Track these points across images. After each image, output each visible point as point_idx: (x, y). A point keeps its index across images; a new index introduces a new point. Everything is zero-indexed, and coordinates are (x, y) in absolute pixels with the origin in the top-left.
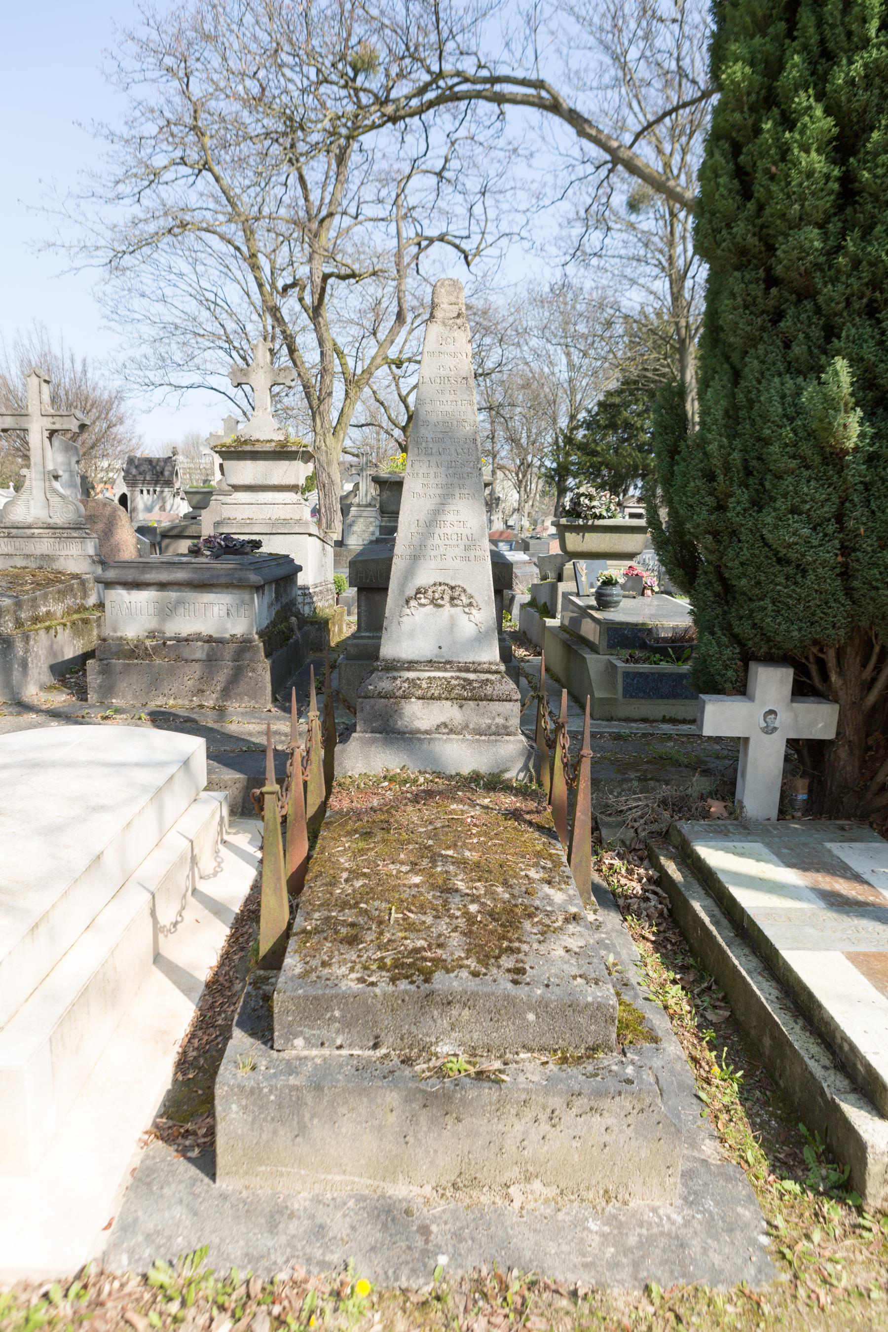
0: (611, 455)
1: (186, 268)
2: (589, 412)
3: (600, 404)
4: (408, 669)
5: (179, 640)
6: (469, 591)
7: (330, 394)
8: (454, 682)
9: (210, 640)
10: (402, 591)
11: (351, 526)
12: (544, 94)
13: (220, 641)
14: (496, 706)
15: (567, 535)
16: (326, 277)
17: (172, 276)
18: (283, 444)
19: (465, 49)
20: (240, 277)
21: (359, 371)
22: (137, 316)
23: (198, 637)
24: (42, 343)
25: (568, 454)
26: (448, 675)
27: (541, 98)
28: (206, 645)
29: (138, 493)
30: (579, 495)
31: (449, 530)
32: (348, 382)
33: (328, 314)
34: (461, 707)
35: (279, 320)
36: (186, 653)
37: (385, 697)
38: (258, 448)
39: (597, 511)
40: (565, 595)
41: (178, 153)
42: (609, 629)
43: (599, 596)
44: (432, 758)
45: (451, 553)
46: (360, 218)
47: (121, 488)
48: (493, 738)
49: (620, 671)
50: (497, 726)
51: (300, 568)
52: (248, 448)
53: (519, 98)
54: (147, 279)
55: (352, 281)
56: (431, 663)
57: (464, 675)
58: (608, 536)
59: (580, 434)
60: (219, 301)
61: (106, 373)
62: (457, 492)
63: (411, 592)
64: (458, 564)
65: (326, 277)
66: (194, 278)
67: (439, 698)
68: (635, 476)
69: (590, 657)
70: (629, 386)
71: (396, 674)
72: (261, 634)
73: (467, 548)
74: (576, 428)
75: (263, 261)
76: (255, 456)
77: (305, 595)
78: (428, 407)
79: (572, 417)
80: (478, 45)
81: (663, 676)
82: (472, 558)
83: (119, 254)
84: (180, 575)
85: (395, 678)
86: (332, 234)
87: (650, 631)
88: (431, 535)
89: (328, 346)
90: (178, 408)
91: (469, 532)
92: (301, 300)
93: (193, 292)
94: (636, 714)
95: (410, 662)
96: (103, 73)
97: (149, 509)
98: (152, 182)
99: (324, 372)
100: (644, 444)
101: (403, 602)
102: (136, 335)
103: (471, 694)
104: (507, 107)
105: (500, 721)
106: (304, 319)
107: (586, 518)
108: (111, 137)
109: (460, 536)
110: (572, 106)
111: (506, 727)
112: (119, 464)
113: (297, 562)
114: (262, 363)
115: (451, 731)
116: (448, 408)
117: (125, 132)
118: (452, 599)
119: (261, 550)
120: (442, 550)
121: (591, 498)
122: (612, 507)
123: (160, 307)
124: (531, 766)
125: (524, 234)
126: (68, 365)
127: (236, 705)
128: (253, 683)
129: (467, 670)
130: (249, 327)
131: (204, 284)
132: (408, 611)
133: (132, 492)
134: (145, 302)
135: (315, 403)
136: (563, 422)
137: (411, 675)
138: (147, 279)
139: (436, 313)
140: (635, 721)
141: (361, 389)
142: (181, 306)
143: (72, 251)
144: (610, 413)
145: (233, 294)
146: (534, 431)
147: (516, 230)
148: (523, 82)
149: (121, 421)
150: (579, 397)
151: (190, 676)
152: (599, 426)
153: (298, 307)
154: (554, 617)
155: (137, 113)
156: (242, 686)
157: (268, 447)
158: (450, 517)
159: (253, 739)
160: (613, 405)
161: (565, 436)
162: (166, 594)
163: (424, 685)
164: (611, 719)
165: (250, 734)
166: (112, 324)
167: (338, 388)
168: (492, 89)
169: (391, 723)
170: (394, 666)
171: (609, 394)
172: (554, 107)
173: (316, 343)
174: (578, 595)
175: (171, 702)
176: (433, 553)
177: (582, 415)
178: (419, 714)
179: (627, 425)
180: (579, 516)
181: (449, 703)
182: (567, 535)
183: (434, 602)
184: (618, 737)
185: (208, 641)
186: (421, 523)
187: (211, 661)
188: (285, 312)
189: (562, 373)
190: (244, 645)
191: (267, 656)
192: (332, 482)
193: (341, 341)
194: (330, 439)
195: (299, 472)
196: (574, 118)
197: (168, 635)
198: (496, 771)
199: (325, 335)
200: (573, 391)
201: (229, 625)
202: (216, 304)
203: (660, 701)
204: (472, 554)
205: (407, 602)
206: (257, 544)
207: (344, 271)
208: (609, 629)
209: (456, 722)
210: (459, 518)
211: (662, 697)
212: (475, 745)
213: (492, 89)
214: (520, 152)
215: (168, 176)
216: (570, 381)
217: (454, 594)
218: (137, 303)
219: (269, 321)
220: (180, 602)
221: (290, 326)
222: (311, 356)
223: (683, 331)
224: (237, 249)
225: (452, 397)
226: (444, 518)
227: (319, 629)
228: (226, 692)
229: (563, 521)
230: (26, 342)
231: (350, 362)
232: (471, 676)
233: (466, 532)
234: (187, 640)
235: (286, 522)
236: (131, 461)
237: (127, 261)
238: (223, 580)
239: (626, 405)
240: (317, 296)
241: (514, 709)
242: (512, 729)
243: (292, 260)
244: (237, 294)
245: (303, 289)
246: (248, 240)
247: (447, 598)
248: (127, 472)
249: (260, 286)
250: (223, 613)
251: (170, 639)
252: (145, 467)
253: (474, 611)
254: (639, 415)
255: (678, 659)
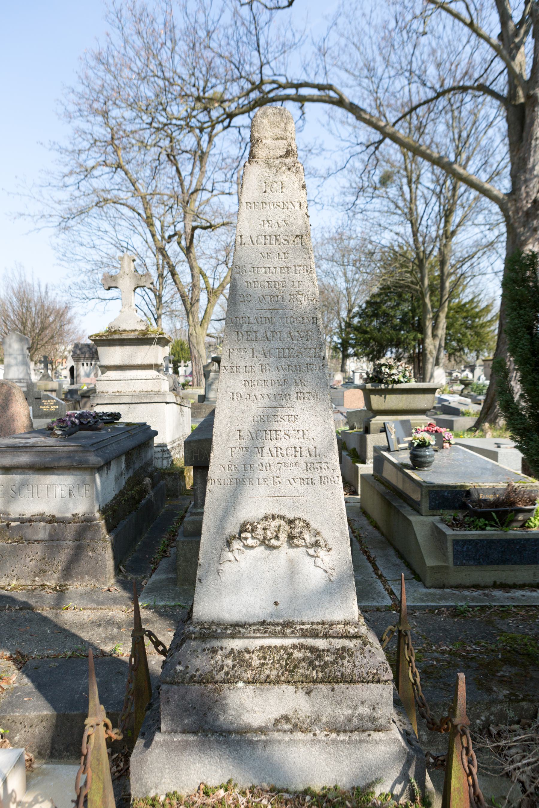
0: (376, 334)
1: (109, 228)
2: (360, 307)
3: (367, 302)
4: (233, 636)
5: (22, 521)
6: (314, 525)
7: (198, 301)
8: (298, 654)
9: (52, 520)
10: (221, 529)
11: (210, 385)
12: (332, 94)
13: (62, 521)
14: (359, 691)
15: (372, 397)
16: (194, 229)
17: (100, 233)
18: (144, 333)
19: (278, 73)
20: (143, 233)
21: (216, 286)
22: (78, 257)
23: (41, 518)
24: (21, 276)
25: (348, 333)
26: (288, 642)
27: (330, 97)
28: (49, 525)
29: (80, 365)
30: (381, 365)
31: (283, 443)
32: (209, 293)
33: (196, 251)
34: (308, 693)
35: (165, 256)
36: (29, 533)
37: (200, 682)
38: (124, 336)
39: (396, 378)
40: (376, 449)
41: (103, 158)
42: (430, 492)
43: (414, 457)
44: (271, 767)
45: (287, 474)
46: (215, 192)
47: (70, 363)
48: (356, 736)
49: (449, 539)
50: (361, 718)
51: (156, 433)
52: (117, 337)
53: (315, 98)
54: (84, 235)
55: (210, 230)
56: (264, 626)
57: (310, 642)
58: (404, 397)
59: (356, 321)
60: (129, 247)
61: (59, 292)
62: (293, 390)
63: (232, 529)
64: (298, 488)
65: (194, 229)
66: (114, 234)
67: (277, 682)
68: (391, 346)
69: (414, 519)
70: (385, 290)
71: (216, 644)
72: (103, 511)
73: (309, 467)
74: (353, 317)
75: (158, 224)
76: (122, 342)
77: (163, 451)
78: (250, 277)
79: (349, 311)
80: (286, 71)
81: (490, 543)
82: (317, 480)
83: (65, 219)
84: (24, 459)
85: (214, 651)
86: (197, 203)
87: (468, 493)
88: (259, 450)
89: (196, 271)
90: (104, 313)
91: (310, 444)
92: (179, 243)
93: (114, 242)
94: (467, 581)
95: (235, 625)
96: (57, 114)
97: (88, 375)
98: (86, 176)
99: (194, 286)
100: (397, 325)
101: (221, 543)
102: (77, 269)
103: (319, 669)
104: (307, 104)
105: (365, 710)
106: (182, 256)
107: (387, 383)
108: (62, 150)
109: (298, 451)
110: (351, 100)
111: (373, 720)
112: (70, 347)
113: (152, 428)
114: (127, 271)
115: (296, 728)
116: (277, 277)
117: (70, 148)
118: (291, 537)
119: (120, 420)
120: (275, 470)
121: (390, 367)
122: (407, 374)
123: (93, 251)
124: (411, 774)
125: (317, 200)
126: (36, 288)
127: (77, 584)
128: (93, 562)
129: (315, 635)
130: (148, 261)
131: (120, 237)
132: (230, 556)
133: (77, 364)
134: (83, 249)
135: (189, 306)
136: (344, 314)
137: (236, 644)
138: (84, 235)
139: (256, 151)
140: (468, 587)
141: (217, 297)
142: (105, 250)
143: (35, 218)
144: (374, 309)
145: (137, 242)
146: (326, 319)
147: (312, 198)
148: (320, 87)
149: (69, 322)
150: (353, 299)
151: (32, 557)
152: (367, 316)
153: (178, 249)
154: (364, 462)
155: (77, 135)
156: (83, 566)
157: (132, 336)
158: (284, 425)
159: (85, 635)
160: (376, 303)
161: (346, 322)
162: (10, 477)
163: (256, 663)
164: (443, 587)
165: (83, 626)
166: (63, 263)
167: (203, 297)
168: (298, 93)
169: (210, 718)
170: (214, 632)
171: (373, 296)
172: (340, 102)
173: (189, 270)
174: (388, 450)
175: (14, 583)
176: (262, 475)
177: (356, 309)
178: (249, 705)
179: (386, 314)
180: (381, 381)
181: (291, 688)
182: (372, 397)
183: (264, 542)
184: (456, 612)
185: (50, 522)
186: (245, 434)
187: (53, 542)
188: (170, 253)
189: (342, 284)
190: (86, 523)
191: (109, 531)
192: (200, 356)
193: (204, 268)
194: (198, 328)
195: (158, 354)
196: (353, 109)
197: (12, 516)
198: (362, 784)
199: (194, 264)
200: (349, 294)
201: (71, 505)
202: (128, 249)
203: (489, 567)
204: (316, 475)
205: (229, 543)
206: (117, 416)
207: (205, 224)
208: (430, 492)
209: (302, 715)
210: (295, 426)
211: (492, 563)
212: (331, 748)
213: (298, 93)
214: (313, 151)
215: (96, 173)
216: (347, 289)
217: (294, 530)
218: (80, 250)
219: (161, 257)
220: (24, 484)
221: (172, 259)
222: (185, 278)
223: (421, 254)
224: (139, 214)
225: (281, 263)
226: (276, 426)
227: (175, 479)
228: (68, 572)
229: (369, 386)
230: (11, 276)
231: (211, 281)
232: (321, 644)
233: (307, 444)
234: (30, 521)
235: (147, 393)
236: (76, 346)
237: (71, 223)
238: (63, 463)
239: (383, 302)
240: (188, 241)
241: (385, 692)
242: (382, 722)
243: (173, 221)
244: (139, 241)
245: (180, 237)
246: (146, 209)
247: (283, 536)
248: (74, 352)
249: (153, 236)
250: (65, 493)
251: (14, 520)
252: (86, 349)
253: (322, 553)
254: (392, 308)
255: (502, 525)
